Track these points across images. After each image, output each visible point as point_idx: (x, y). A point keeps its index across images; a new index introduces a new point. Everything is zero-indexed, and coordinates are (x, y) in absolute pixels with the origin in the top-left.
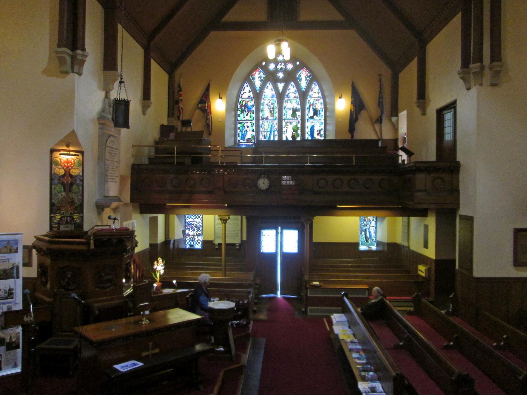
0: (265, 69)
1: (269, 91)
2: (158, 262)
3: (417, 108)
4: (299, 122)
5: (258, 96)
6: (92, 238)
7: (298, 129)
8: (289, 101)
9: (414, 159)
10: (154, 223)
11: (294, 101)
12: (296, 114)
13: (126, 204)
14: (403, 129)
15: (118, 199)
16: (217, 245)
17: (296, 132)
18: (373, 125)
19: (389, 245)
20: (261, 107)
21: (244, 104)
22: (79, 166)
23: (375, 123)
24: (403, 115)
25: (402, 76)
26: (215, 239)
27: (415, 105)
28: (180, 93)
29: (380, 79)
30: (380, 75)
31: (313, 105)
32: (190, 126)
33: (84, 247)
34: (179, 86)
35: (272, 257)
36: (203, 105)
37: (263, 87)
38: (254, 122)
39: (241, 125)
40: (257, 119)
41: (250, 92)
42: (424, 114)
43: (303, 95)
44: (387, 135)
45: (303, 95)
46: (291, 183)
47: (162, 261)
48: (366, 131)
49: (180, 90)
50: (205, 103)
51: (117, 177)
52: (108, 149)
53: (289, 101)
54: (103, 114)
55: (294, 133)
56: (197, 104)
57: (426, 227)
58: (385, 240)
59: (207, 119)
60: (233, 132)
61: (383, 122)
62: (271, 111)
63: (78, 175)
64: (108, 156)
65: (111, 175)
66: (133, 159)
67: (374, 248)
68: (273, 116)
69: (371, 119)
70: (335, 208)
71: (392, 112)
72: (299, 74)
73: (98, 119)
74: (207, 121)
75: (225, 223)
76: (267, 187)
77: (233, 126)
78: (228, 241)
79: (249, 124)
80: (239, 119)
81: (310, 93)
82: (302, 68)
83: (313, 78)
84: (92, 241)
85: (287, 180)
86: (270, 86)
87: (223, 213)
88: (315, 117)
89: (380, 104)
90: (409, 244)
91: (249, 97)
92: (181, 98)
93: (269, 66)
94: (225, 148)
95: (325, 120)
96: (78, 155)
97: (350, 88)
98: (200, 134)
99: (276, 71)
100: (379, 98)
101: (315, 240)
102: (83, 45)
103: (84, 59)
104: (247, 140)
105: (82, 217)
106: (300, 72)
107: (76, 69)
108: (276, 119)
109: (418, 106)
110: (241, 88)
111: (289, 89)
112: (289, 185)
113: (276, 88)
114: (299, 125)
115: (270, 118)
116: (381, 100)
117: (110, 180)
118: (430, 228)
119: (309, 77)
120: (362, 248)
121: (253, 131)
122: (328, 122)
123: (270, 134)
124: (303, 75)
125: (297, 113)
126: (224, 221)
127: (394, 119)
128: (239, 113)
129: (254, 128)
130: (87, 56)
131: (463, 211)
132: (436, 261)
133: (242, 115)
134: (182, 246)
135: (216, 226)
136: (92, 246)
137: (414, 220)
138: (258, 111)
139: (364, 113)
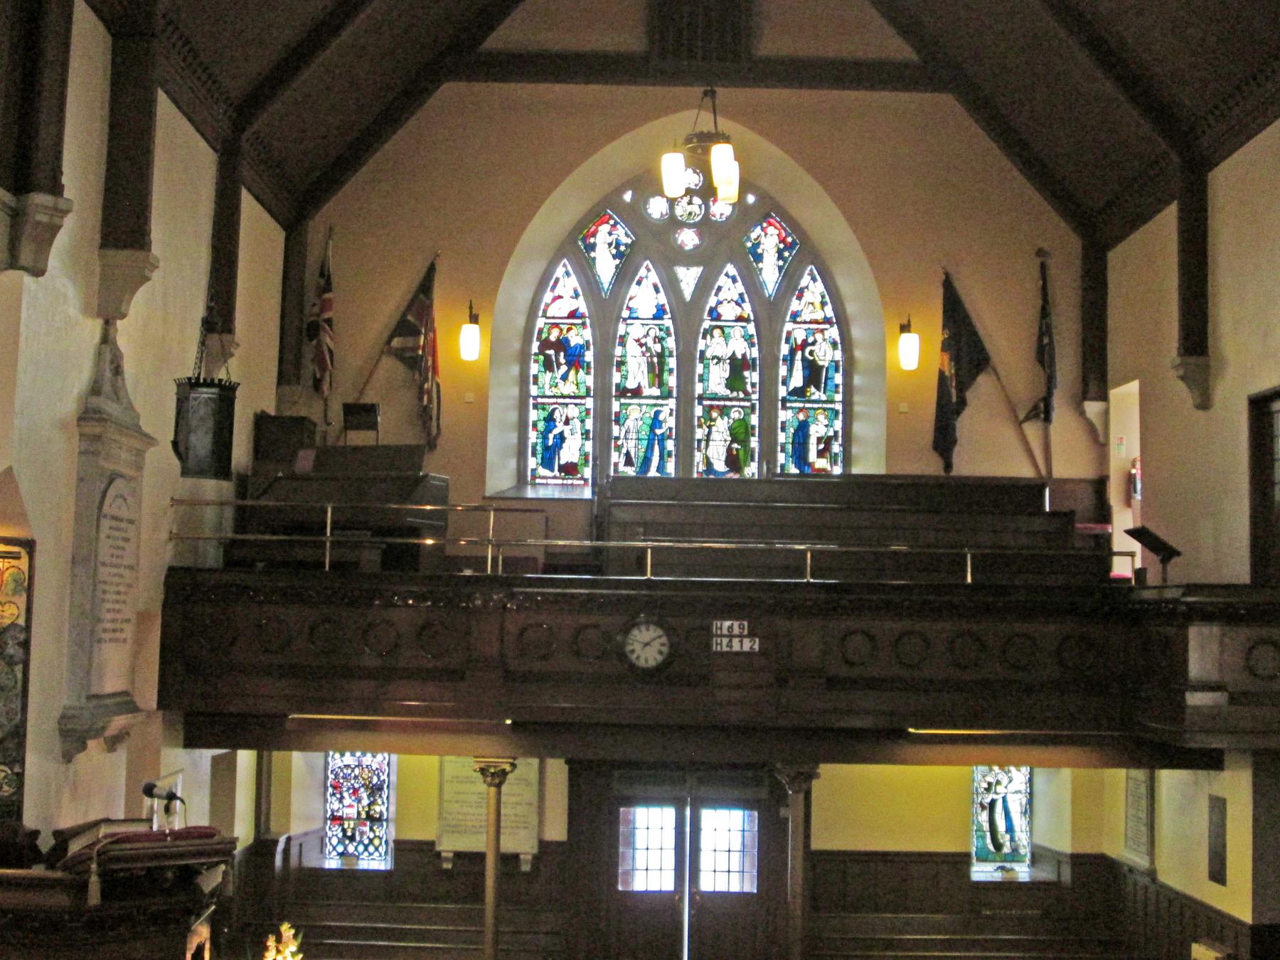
0: (634, 217)
1: (645, 296)
2: (279, 940)
3: (1181, 385)
4: (753, 408)
5: (606, 309)
6: (94, 866)
7: (749, 430)
8: (717, 332)
9: (1179, 572)
10: (223, 774)
11: (737, 332)
13: (149, 714)
14: (1126, 447)
15: (126, 703)
16: (447, 859)
17: (745, 443)
19: (1078, 860)
20: (618, 351)
21: (553, 338)
22: (15, 592)
23: (1027, 418)
24: (1126, 395)
25: (1122, 261)
26: (439, 837)
27: (1173, 374)
28: (327, 296)
29: (1043, 267)
30: (1040, 253)
32: (373, 426)
33: (60, 900)
34: (324, 274)
35: (664, 905)
36: (410, 342)
37: (625, 275)
38: (589, 403)
39: (543, 414)
40: (602, 393)
41: (576, 296)
42: (1204, 403)
44: (1070, 464)
45: (768, 314)
47: (295, 936)
48: (992, 449)
49: (328, 287)
50: (417, 333)
51: (128, 621)
52: (106, 524)
53: (717, 332)
54: (95, 401)
55: (735, 446)
56: (386, 336)
57: (1218, 806)
58: (1065, 845)
59: (421, 391)
60: (513, 438)
61: (1055, 415)
62: (651, 366)
63: (13, 625)
64: (104, 553)
65: (109, 616)
66: (170, 546)
67: (1023, 872)
68: (661, 384)
69: (1013, 411)
70: (898, 734)
71: (1085, 381)
72: (753, 236)
73: (80, 419)
74: (421, 399)
75: (499, 786)
76: (660, 658)
77: (513, 416)
78: (508, 846)
79: (573, 411)
80: (534, 390)
81: (795, 305)
82: (766, 217)
83: (802, 253)
84: (94, 879)
85: (732, 637)
86: (649, 274)
87: (492, 750)
89: (1044, 355)
90: (1152, 862)
91: (573, 315)
92: (326, 316)
93: (646, 202)
94: (484, 498)
95: (847, 403)
96: (16, 557)
98: (412, 456)
99: (674, 223)
100: (1041, 336)
101: (816, 845)
102: (57, 172)
103: (56, 220)
104: (561, 468)
105: (20, 776)
106: (758, 230)
107: (26, 256)
108: (669, 395)
109: (1182, 378)
110: (545, 280)
111: (720, 289)
112: (737, 654)
113: (671, 285)
114: (754, 420)
115: (647, 391)
116: (1046, 341)
117: (106, 636)
118: (1230, 810)
120: (982, 872)
121: (586, 435)
122: (857, 409)
123: (650, 448)
124: (769, 240)
126: (497, 778)
128: (534, 368)
129: (589, 424)
130: (67, 212)
132: (1257, 931)
133: (546, 378)
134: (311, 861)
135: (446, 787)
136: (94, 896)
137: (1170, 780)
138: (607, 363)
139: (984, 383)
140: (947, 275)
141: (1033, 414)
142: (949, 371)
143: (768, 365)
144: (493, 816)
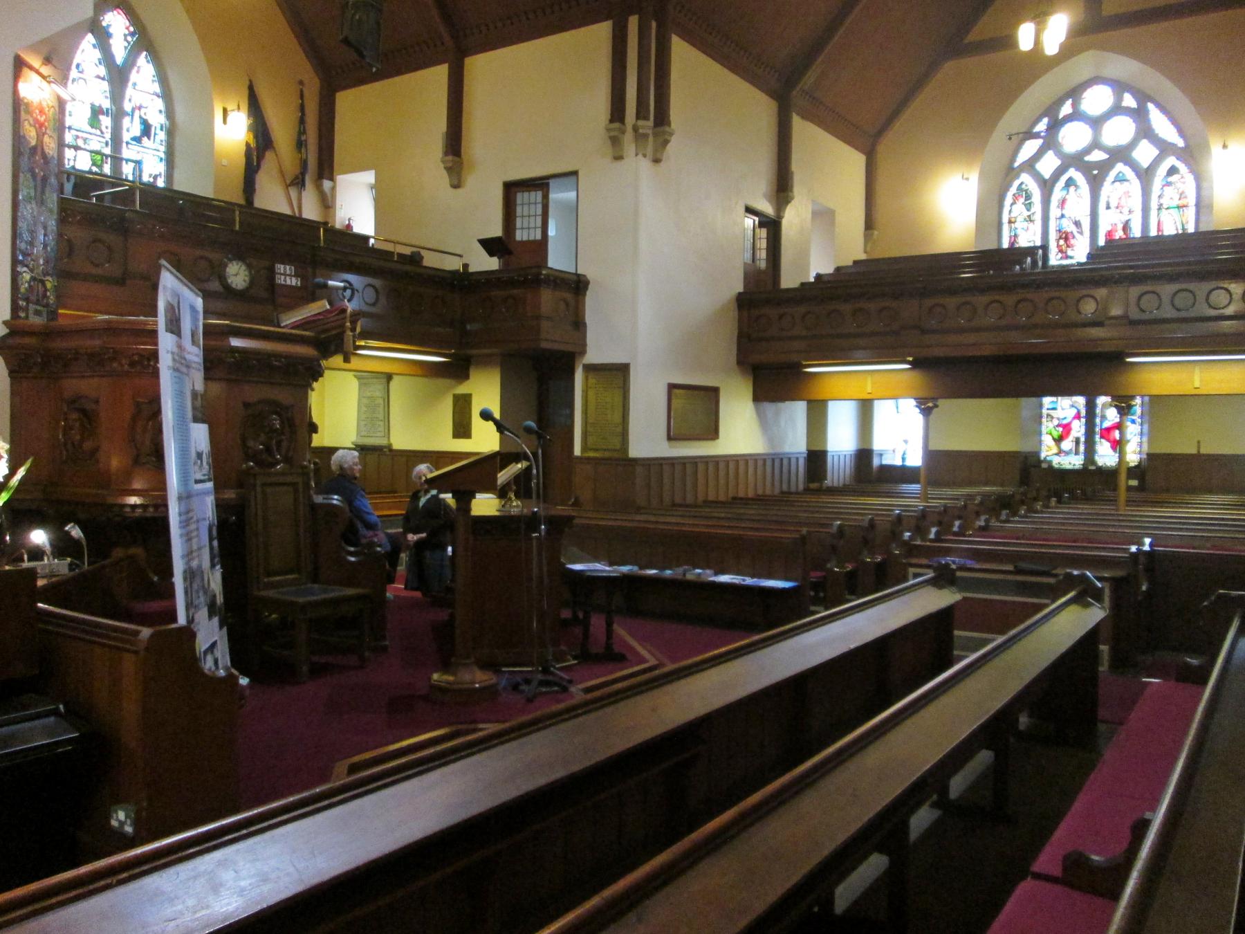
12: (99, 121)
18: (287, 186)
29: (302, 91)
31: (140, 108)
43: (118, 77)
45: (118, 77)
46: (294, 282)
48: (273, 197)
83: (143, 41)
88: (145, 139)
97: (246, 92)
119: (132, 34)
125: (101, 117)
127: (327, 184)
131: (596, 353)
139: (269, 155)
140: (251, 81)
141: (292, 184)
142: (253, 145)
143: (118, 115)
144: (881, 199)
